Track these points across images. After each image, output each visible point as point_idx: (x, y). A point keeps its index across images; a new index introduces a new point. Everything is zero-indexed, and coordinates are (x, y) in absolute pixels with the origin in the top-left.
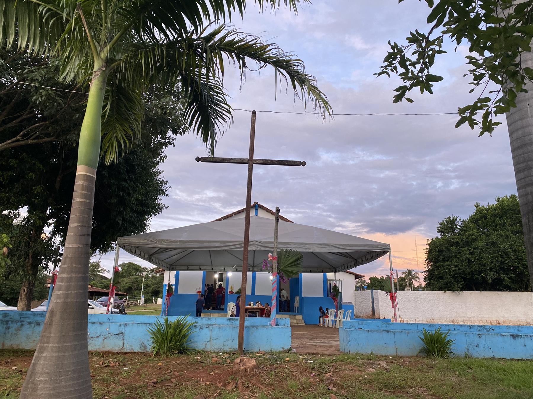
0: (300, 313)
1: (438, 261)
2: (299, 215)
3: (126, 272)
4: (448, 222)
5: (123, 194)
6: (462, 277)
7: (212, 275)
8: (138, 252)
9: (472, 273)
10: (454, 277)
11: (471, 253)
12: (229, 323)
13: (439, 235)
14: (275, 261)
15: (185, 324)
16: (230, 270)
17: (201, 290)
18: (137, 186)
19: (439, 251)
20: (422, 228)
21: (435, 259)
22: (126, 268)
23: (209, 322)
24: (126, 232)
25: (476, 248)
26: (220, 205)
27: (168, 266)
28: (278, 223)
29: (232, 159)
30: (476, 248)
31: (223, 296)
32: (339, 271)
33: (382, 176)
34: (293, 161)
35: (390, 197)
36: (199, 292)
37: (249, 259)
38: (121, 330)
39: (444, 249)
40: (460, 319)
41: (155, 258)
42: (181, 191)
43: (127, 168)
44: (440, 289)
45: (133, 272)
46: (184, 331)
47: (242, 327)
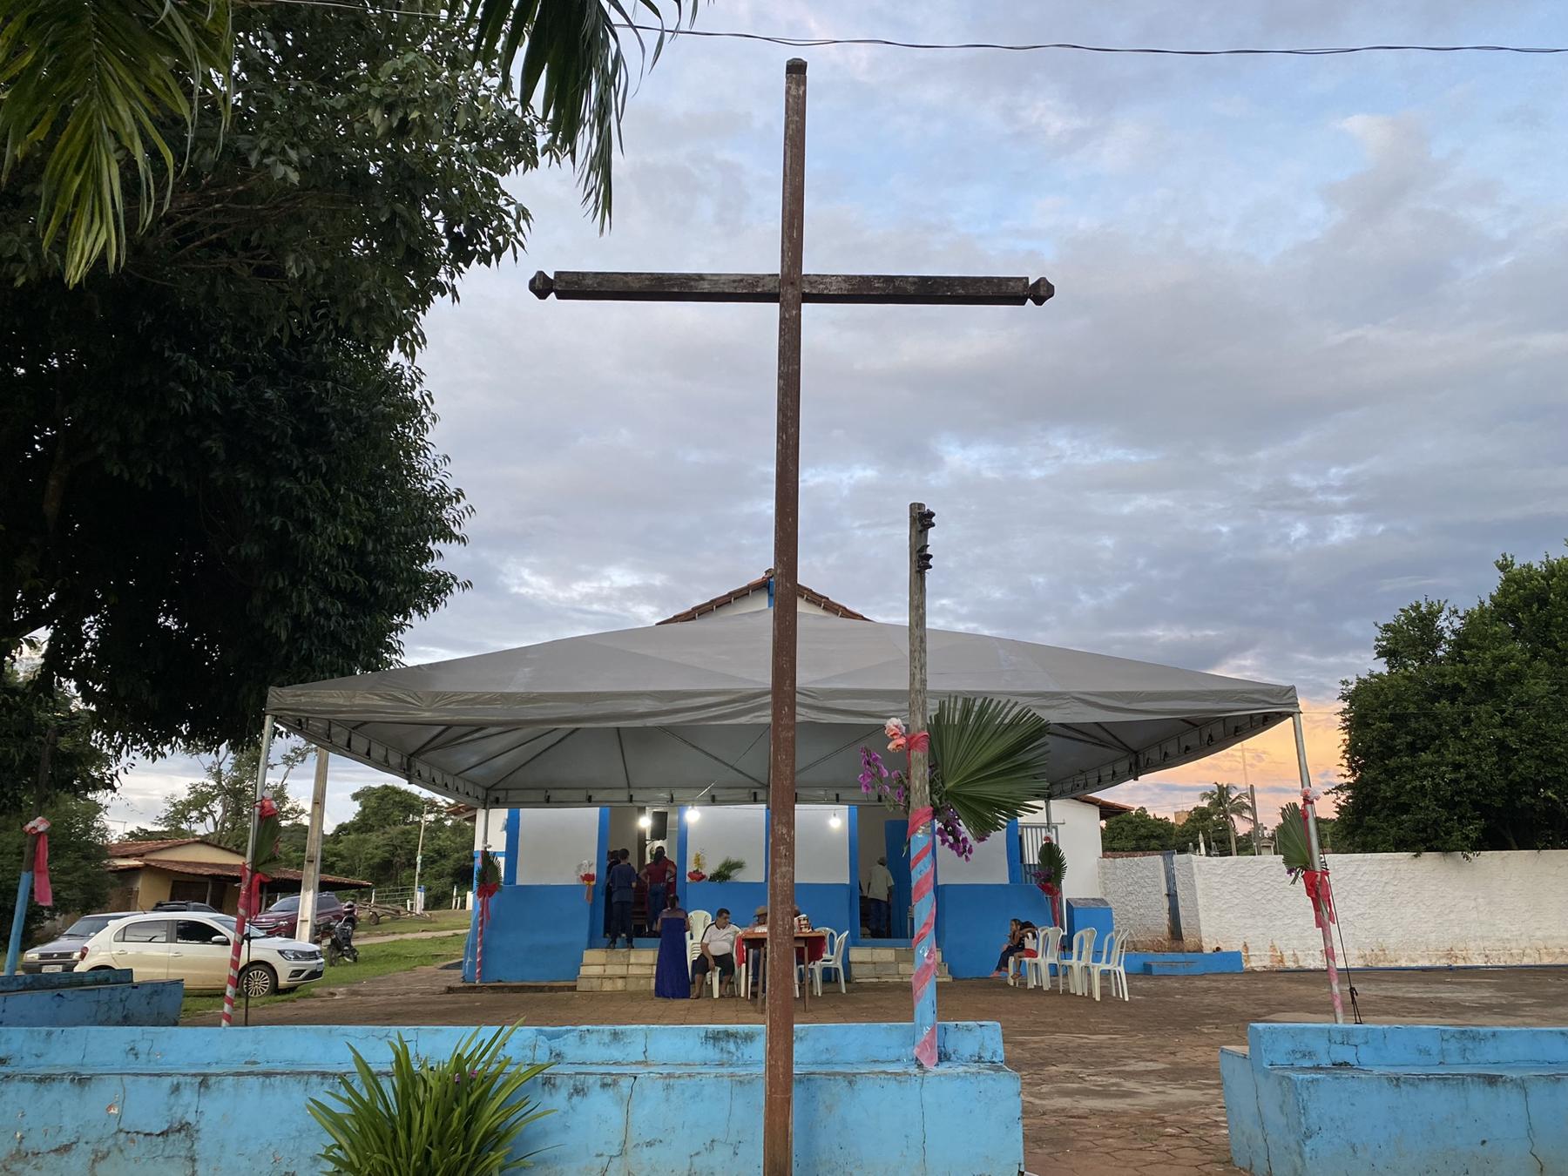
1: (1392, 752)
4: (1411, 621)
5: (284, 525)
6: (1476, 805)
7: (633, 819)
8: (360, 743)
9: (1513, 790)
10: (1449, 805)
11: (1505, 723)
12: (711, 1053)
13: (1381, 667)
15: (495, 1077)
16: (694, 802)
17: (593, 871)
18: (336, 495)
19: (1392, 718)
20: (1248, 662)
21: (1381, 743)
22: (373, 803)
23: (616, 1053)
24: (303, 671)
25: (1523, 704)
26: (653, 609)
27: (481, 793)
28: (923, 579)
29: (701, 277)
30: (1523, 704)
31: (671, 887)
32: (1061, 795)
33: (1127, 509)
34: (989, 280)
35: (1154, 573)
36: (588, 877)
37: (781, 747)
38: (178, 1112)
39: (1412, 709)
40: (1472, 944)
41: (431, 765)
42: (537, 571)
43: (295, 428)
44: (1400, 846)
45: (397, 814)
46: (488, 1118)
47: (782, 1082)
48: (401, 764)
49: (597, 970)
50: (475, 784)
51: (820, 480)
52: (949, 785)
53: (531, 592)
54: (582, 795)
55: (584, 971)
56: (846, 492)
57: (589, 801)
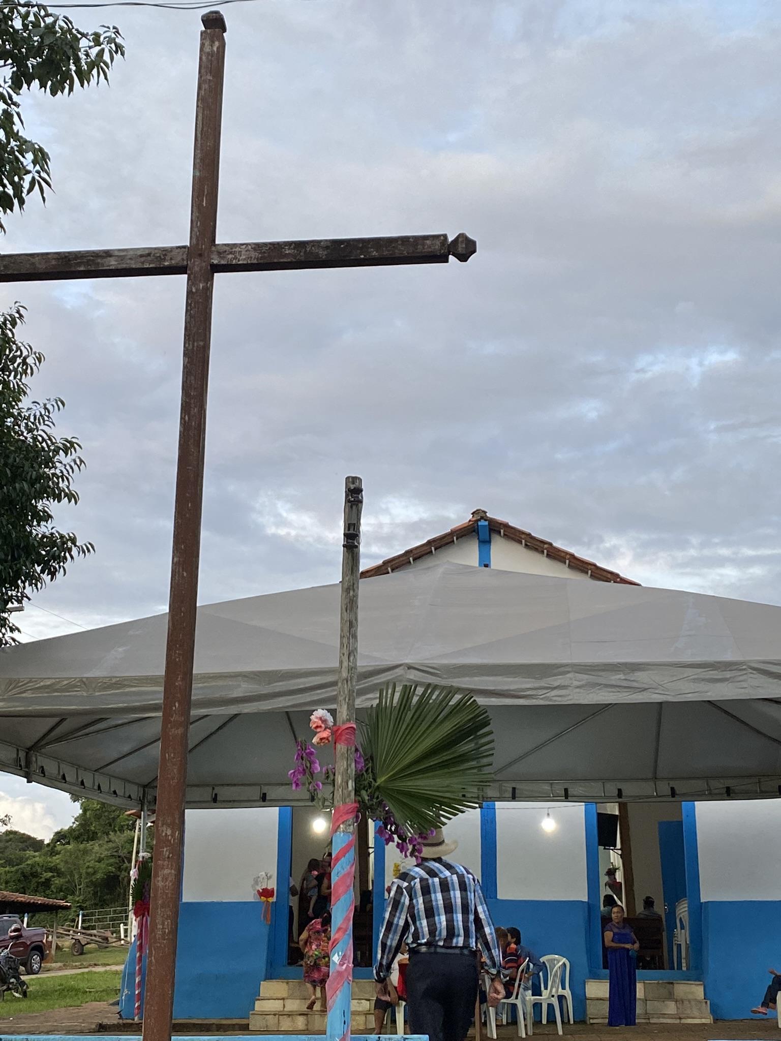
0: (697, 973)
2: (757, 571)
3: (98, 817)
14: (341, 747)
17: (272, 884)
27: (134, 791)
29: (108, 254)
36: (266, 893)
42: (300, 505)
48: (18, 760)
49: (276, 1006)
50: (126, 780)
51: (657, 369)
52: (380, 781)
53: (293, 533)
54: (255, 793)
55: (259, 1006)
56: (695, 384)
57: (264, 800)
